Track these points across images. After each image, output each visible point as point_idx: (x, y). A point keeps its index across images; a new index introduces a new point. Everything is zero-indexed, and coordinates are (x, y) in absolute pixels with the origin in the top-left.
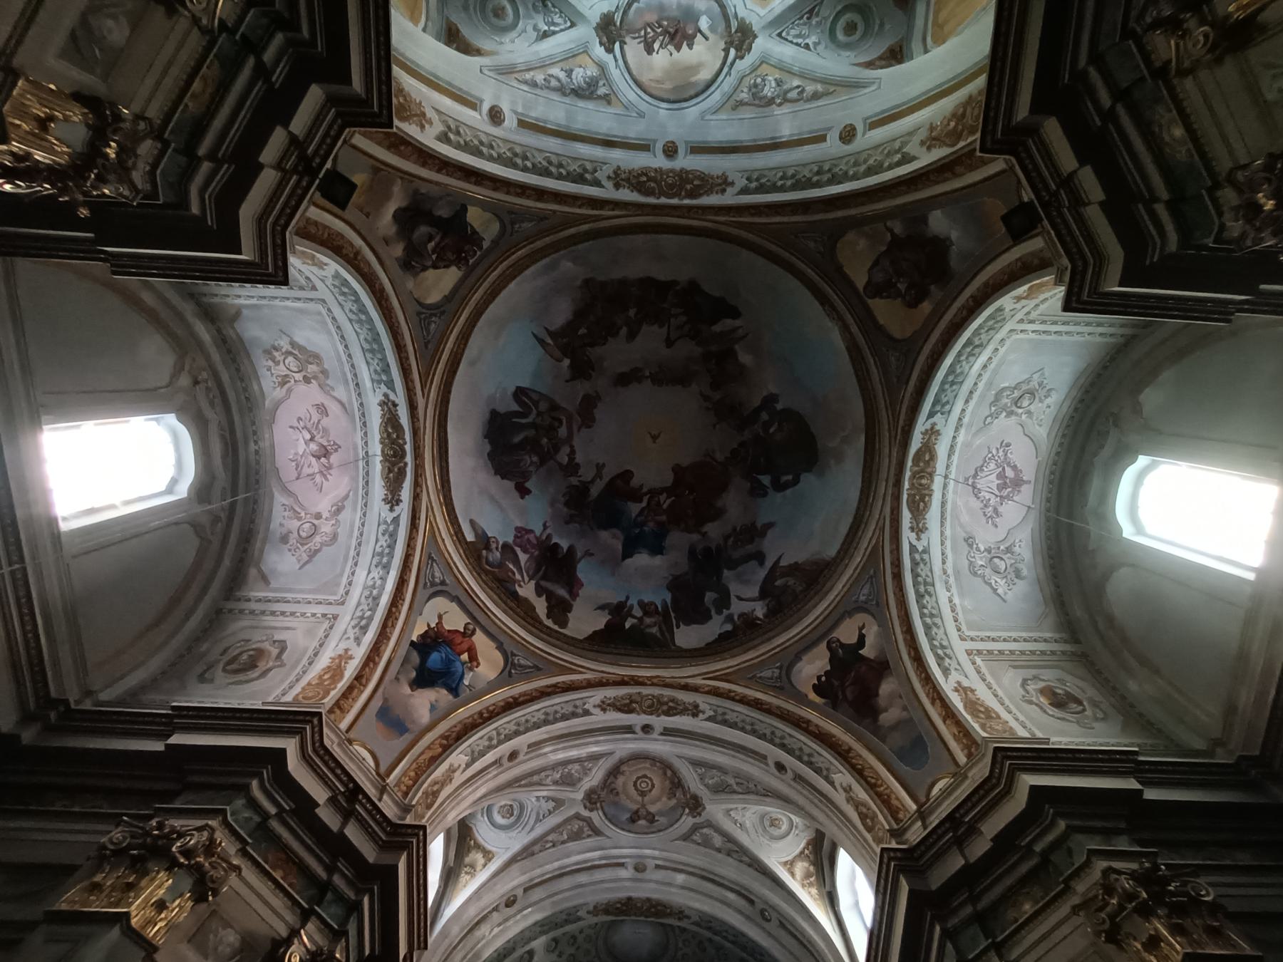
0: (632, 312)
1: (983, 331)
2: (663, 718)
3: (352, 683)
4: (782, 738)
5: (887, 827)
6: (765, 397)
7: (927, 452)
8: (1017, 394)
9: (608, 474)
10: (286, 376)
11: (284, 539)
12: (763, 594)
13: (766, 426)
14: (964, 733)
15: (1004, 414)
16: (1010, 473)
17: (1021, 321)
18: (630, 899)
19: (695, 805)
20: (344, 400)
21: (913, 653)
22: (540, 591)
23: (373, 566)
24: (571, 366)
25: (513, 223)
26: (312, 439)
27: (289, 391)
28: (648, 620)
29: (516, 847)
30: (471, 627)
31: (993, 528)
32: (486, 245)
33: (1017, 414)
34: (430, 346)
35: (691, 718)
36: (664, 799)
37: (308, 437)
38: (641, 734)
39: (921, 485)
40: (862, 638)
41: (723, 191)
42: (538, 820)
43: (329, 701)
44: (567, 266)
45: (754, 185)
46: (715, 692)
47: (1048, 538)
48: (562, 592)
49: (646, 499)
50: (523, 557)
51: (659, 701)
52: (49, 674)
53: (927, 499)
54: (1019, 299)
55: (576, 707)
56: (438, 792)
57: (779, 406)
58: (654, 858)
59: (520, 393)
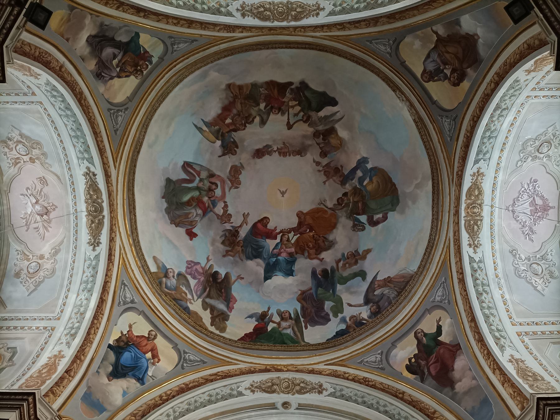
0: (262, 106)
1: (507, 98)
2: (297, 395)
4: (385, 406)
6: (359, 160)
7: (476, 187)
8: (538, 143)
9: (252, 221)
10: (18, 158)
11: (17, 275)
12: (367, 301)
13: (361, 180)
14: (517, 392)
15: (530, 158)
16: (539, 201)
17: (534, 89)
20: (59, 174)
21: (477, 337)
22: (205, 306)
24: (223, 146)
25: (173, 44)
26: (37, 202)
27: (20, 169)
28: (284, 324)
30: (153, 333)
31: (530, 242)
32: (155, 60)
33: (539, 158)
34: (118, 132)
37: (34, 201)
38: (282, 409)
39: (474, 213)
40: (439, 328)
41: (318, 14)
43: (45, 388)
44: (214, 75)
45: (339, 8)
46: (335, 375)
48: (222, 306)
49: (279, 237)
50: (193, 282)
53: (479, 223)
54: (529, 72)
55: (232, 389)
57: (369, 166)
59: (187, 166)
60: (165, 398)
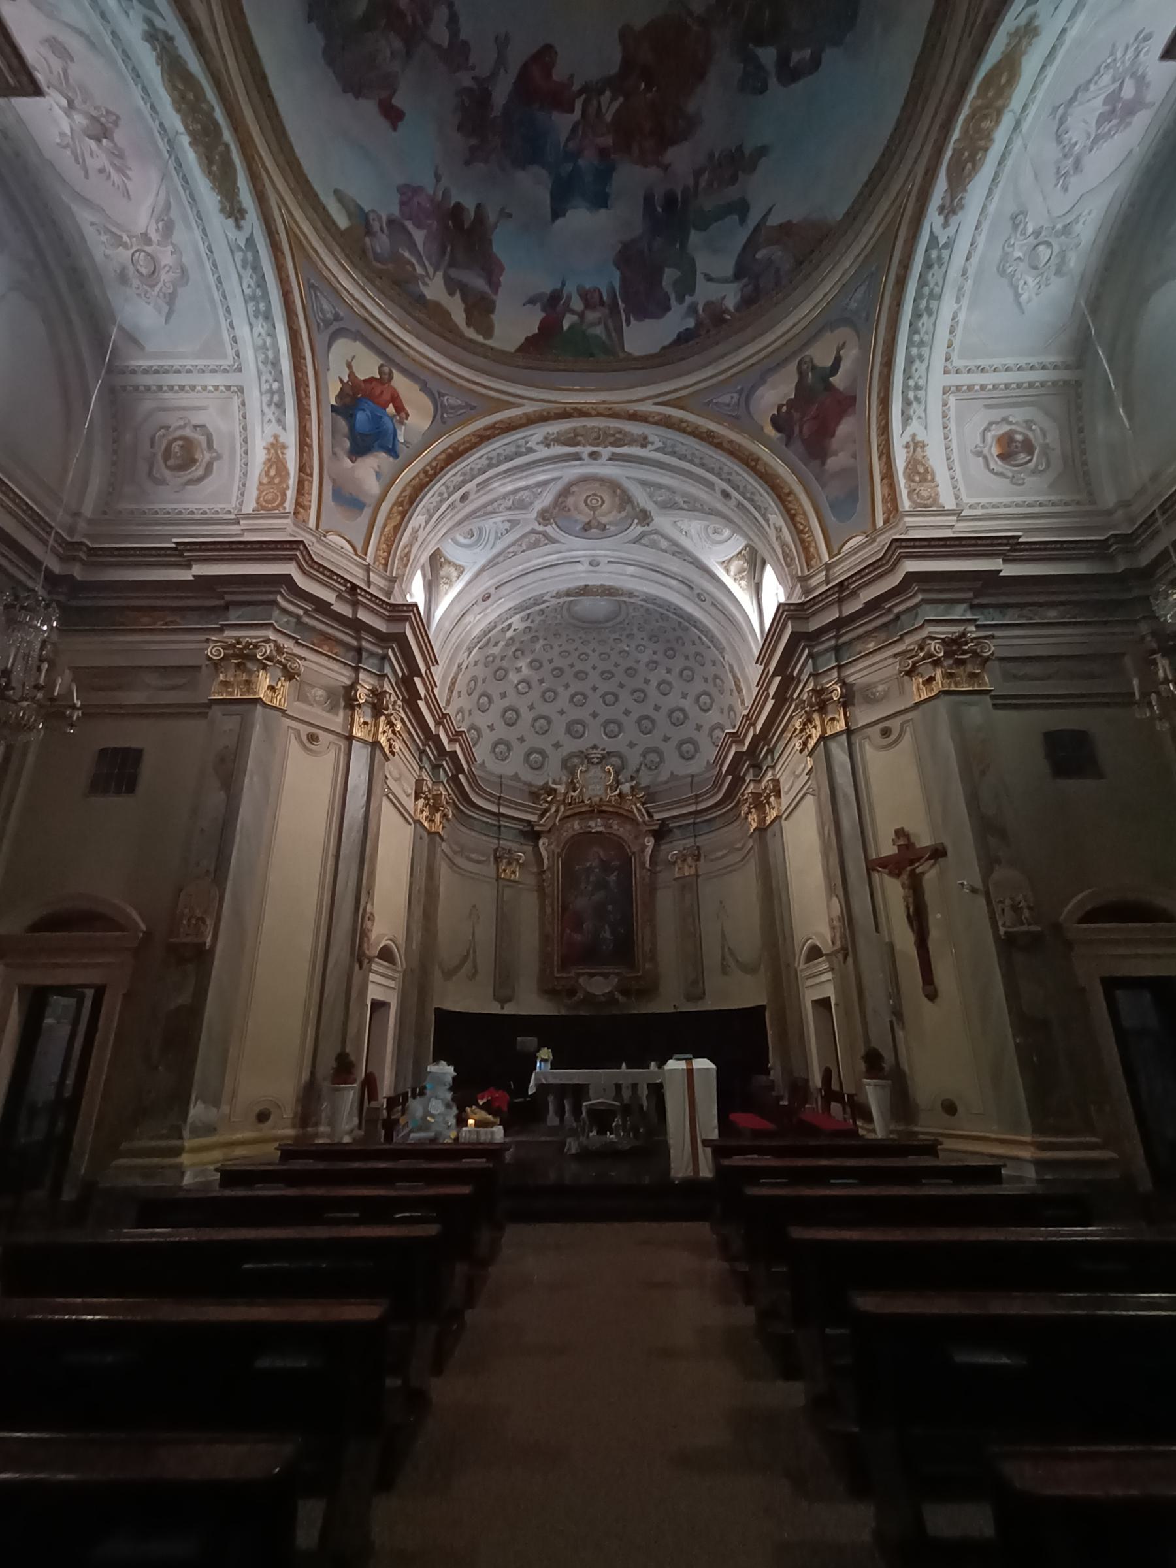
3: (299, 476)
4: (730, 474)
5: (800, 574)
7: (1010, 65)
11: (123, 278)
18: (586, 586)
19: (644, 517)
21: (882, 395)
22: (452, 286)
23: (253, 319)
28: (591, 316)
29: (482, 562)
30: (386, 369)
35: (639, 448)
36: (614, 512)
40: (838, 360)
42: (497, 538)
46: (667, 423)
47: (1132, 205)
48: (479, 283)
50: (419, 236)
51: (605, 433)
52: (35, 507)
55: (519, 446)
56: (409, 552)
58: (605, 556)
60: (431, 472)
